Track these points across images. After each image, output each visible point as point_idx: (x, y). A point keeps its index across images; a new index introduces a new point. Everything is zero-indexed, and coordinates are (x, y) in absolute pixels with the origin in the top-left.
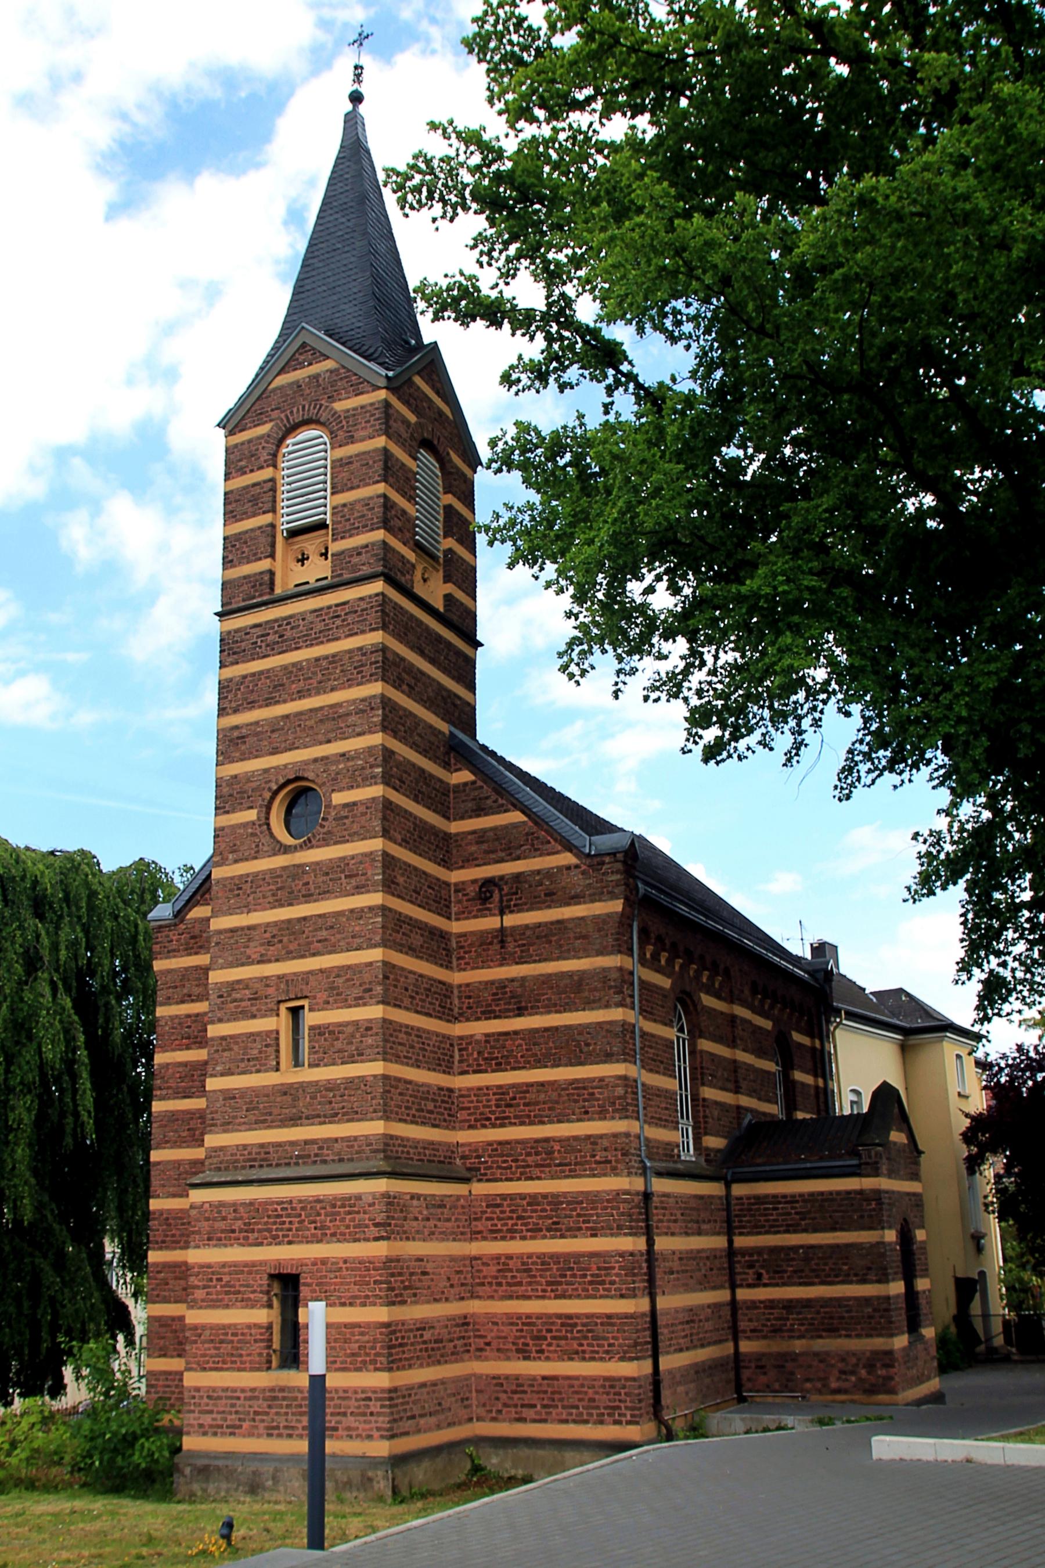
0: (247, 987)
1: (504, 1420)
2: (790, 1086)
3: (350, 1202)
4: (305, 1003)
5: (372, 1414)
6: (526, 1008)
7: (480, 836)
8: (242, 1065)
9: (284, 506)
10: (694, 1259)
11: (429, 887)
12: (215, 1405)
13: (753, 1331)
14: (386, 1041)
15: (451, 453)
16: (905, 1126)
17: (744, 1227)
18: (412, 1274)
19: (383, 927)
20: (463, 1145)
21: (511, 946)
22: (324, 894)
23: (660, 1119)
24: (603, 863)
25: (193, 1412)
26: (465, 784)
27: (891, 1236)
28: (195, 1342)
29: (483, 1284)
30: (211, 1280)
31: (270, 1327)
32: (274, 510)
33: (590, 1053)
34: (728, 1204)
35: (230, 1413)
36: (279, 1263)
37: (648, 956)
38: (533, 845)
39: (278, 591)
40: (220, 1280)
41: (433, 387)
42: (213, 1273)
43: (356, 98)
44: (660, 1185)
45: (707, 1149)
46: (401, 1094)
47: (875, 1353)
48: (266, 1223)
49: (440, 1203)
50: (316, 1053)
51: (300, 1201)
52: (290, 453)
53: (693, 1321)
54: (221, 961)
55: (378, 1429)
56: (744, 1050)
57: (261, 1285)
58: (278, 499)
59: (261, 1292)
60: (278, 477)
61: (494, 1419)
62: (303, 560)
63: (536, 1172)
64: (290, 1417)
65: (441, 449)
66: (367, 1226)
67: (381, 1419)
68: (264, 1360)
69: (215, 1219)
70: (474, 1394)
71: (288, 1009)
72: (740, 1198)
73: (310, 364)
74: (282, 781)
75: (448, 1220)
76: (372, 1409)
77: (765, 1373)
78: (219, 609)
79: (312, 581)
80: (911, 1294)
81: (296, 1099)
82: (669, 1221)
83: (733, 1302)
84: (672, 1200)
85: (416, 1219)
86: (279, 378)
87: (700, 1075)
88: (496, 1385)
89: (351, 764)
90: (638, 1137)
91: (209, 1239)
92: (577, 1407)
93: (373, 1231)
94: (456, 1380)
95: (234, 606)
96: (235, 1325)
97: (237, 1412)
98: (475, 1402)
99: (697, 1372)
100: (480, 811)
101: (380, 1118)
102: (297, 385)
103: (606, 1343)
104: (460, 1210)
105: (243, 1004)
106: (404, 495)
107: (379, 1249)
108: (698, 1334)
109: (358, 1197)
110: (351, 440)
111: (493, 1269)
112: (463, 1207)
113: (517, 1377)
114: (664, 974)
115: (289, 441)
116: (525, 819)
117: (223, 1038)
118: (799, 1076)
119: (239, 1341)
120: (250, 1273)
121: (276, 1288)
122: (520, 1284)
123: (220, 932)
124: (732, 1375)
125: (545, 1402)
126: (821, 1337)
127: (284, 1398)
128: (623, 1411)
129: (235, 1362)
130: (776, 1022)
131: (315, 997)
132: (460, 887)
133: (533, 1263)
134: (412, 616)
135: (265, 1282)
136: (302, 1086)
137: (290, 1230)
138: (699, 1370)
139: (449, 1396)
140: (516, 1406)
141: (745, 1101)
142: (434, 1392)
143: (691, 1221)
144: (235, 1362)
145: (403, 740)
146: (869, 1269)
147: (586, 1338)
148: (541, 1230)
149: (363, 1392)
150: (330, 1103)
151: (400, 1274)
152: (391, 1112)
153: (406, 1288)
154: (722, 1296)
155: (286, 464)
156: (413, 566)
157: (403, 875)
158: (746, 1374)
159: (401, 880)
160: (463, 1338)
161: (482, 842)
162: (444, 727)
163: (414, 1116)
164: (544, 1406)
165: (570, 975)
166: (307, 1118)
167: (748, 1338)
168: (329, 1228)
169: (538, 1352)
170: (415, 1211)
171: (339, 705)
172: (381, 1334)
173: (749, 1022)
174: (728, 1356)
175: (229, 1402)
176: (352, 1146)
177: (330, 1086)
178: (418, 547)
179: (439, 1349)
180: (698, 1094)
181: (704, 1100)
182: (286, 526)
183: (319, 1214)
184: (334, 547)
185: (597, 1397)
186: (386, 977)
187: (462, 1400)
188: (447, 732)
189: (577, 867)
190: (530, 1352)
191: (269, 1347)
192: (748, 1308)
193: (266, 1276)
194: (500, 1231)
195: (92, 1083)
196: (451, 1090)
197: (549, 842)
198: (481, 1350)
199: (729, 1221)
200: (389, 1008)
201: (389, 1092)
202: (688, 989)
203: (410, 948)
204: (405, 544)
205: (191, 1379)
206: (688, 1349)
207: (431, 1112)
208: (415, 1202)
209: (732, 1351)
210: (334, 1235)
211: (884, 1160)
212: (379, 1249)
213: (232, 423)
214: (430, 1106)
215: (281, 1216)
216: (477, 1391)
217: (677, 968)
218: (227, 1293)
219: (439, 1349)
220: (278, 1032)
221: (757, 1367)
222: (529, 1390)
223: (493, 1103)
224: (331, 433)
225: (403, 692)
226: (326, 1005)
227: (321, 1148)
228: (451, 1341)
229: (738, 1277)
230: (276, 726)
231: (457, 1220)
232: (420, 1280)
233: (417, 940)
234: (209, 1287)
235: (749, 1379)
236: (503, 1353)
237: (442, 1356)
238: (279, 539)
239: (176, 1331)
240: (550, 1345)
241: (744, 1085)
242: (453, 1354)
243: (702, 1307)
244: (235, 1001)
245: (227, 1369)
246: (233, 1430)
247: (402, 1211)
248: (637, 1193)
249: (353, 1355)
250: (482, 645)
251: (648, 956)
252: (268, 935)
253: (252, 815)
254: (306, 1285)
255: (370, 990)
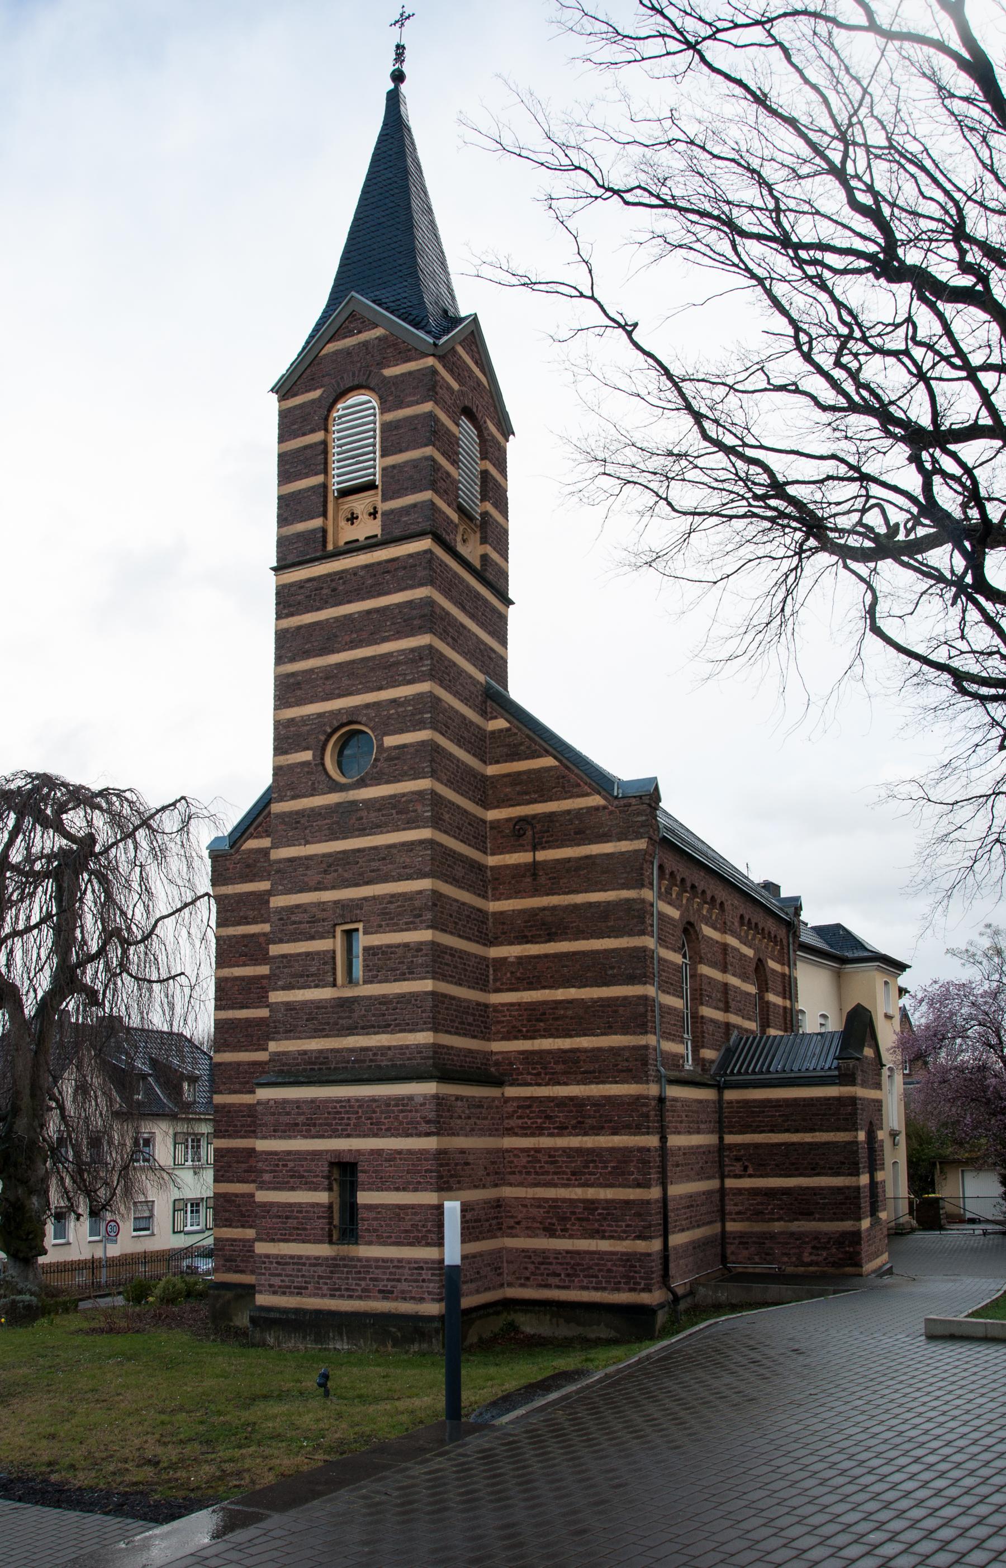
0: (305, 911)
1: (532, 1286)
2: (765, 1007)
3: (403, 1102)
4: (360, 926)
5: (424, 1281)
6: (556, 933)
7: (515, 778)
8: (301, 980)
9: (335, 468)
10: (694, 1154)
11: (470, 824)
12: (283, 1269)
13: (739, 1213)
14: (434, 961)
15: (488, 421)
16: (873, 1043)
17: (733, 1127)
18: (456, 1164)
19: (432, 859)
20: (497, 1053)
21: (543, 879)
22: (377, 828)
23: (669, 1034)
24: (630, 805)
25: (264, 1274)
26: (501, 731)
27: (862, 1136)
28: (264, 1217)
29: (514, 1173)
30: (277, 1165)
31: (330, 1206)
32: (325, 472)
33: (614, 976)
34: (721, 1107)
35: (298, 1276)
36: (338, 1153)
37: (663, 890)
38: (563, 787)
39: (330, 547)
40: (286, 1165)
41: (472, 358)
42: (279, 1160)
43: (398, 77)
44: (674, 1092)
45: (704, 1060)
46: (447, 1009)
47: (844, 1234)
48: (326, 1119)
49: (478, 1104)
50: (370, 970)
51: (357, 1100)
52: (340, 417)
53: (692, 1206)
54: (280, 887)
55: (429, 1293)
56: (733, 975)
57: (322, 1171)
58: (330, 461)
59: (323, 1177)
60: (330, 440)
61: (522, 1285)
62: (352, 519)
63: (563, 1079)
64: (350, 1281)
65: (479, 416)
66: (418, 1123)
67: (432, 1285)
68: (326, 1233)
69: (280, 1114)
70: (505, 1265)
71: (344, 931)
72: (730, 1102)
73: (360, 332)
74: (336, 724)
75: (485, 1118)
76: (424, 1277)
77: (747, 1249)
78: (275, 564)
79: (362, 538)
80: (873, 1184)
81: (352, 1011)
82: (677, 1122)
83: (722, 1191)
84: (679, 1104)
85: (460, 1117)
86: (329, 346)
87: (698, 997)
88: (525, 1257)
89: (400, 709)
90: (655, 1049)
91: (275, 1131)
92: (596, 1277)
93: (424, 1127)
94: (491, 1253)
95: (288, 562)
96: (300, 1204)
97: (303, 1276)
98: (506, 1271)
99: (694, 1248)
100: (514, 756)
101: (428, 1030)
102: (348, 352)
103: (624, 1224)
104: (494, 1110)
105: (302, 926)
106: (448, 458)
107: (431, 1143)
108: (696, 1216)
109: (411, 1098)
110: (400, 405)
111: (524, 1160)
112: (497, 1107)
113: (544, 1251)
114: (674, 906)
115: (339, 406)
116: (557, 763)
117: (284, 956)
118: (772, 998)
119: (304, 1218)
120: (312, 1160)
121: (336, 1175)
122: (547, 1173)
123: (279, 861)
124: (719, 1250)
125: (570, 1271)
126: (797, 1220)
127: (345, 1266)
128: (638, 1280)
129: (301, 1235)
130: (757, 950)
131: (369, 921)
132: (496, 825)
133: (559, 1156)
134: (456, 573)
135: (326, 1168)
136: (355, 1000)
137: (348, 1125)
138: (696, 1246)
139: (485, 1266)
140: (542, 1274)
141: (734, 1019)
142: (474, 1263)
143: (693, 1122)
144: (301, 1235)
145: (447, 688)
146: (844, 1163)
147: (605, 1219)
148: (566, 1128)
149: (415, 1262)
150: (384, 1015)
151: (447, 1165)
152: (439, 1024)
153: (452, 1176)
154: (714, 1184)
155: (336, 428)
156: (456, 526)
157: (448, 812)
158: (730, 1249)
159: (446, 817)
160: (497, 1218)
161: (516, 785)
162: (481, 677)
163: (457, 1028)
164: (568, 1275)
165: (598, 904)
166: (363, 1028)
167: (734, 1220)
168: (384, 1124)
169: (562, 1230)
170: (459, 1110)
171: (390, 654)
172: (432, 1214)
173: (737, 950)
174: (716, 1235)
175: (296, 1267)
176: (404, 1054)
177: (383, 1000)
178: (461, 510)
179: (478, 1227)
180: (697, 1013)
181: (702, 1017)
182: (336, 487)
183: (374, 1112)
184: (383, 507)
185: (614, 1268)
186: (435, 905)
187: (496, 1269)
188: (483, 682)
189: (605, 808)
190: (556, 1230)
191: (330, 1223)
192: (734, 1194)
193: (326, 1164)
194: (529, 1128)
195: (21, 1000)
196: (486, 1006)
197: (579, 785)
198: (512, 1228)
199: (720, 1122)
200: (437, 933)
201: (437, 1006)
202: (692, 920)
203: (454, 879)
204: (449, 505)
205: (262, 1248)
206: (688, 1229)
207: (470, 1024)
208: (459, 1103)
209: (719, 1230)
210: (388, 1130)
211: (860, 1073)
212: (431, 1143)
213: (285, 389)
214: (470, 1019)
215: (340, 1113)
216: (507, 1262)
217: (684, 902)
218: (292, 1177)
219: (478, 1227)
220: (334, 952)
221: (740, 1243)
222: (554, 1261)
223: (525, 1017)
224: (381, 398)
225: (448, 644)
226: (379, 929)
227: (375, 1054)
228: (487, 1220)
229: (727, 1169)
230: (330, 674)
231: (492, 1118)
232: (463, 1170)
233: (459, 872)
234: (275, 1171)
235: (733, 1253)
236: (531, 1232)
237: (480, 1233)
238: (331, 498)
239: (239, 1206)
240: (573, 1224)
241: (732, 1004)
242: (488, 1231)
243: (698, 1194)
244: (294, 923)
245: (294, 1241)
246: (300, 1291)
247: (449, 1111)
248: (654, 1098)
249: (406, 1231)
250: (512, 603)
251: (663, 890)
252: (324, 865)
253: (307, 756)
254: (362, 1171)
255: (421, 916)
